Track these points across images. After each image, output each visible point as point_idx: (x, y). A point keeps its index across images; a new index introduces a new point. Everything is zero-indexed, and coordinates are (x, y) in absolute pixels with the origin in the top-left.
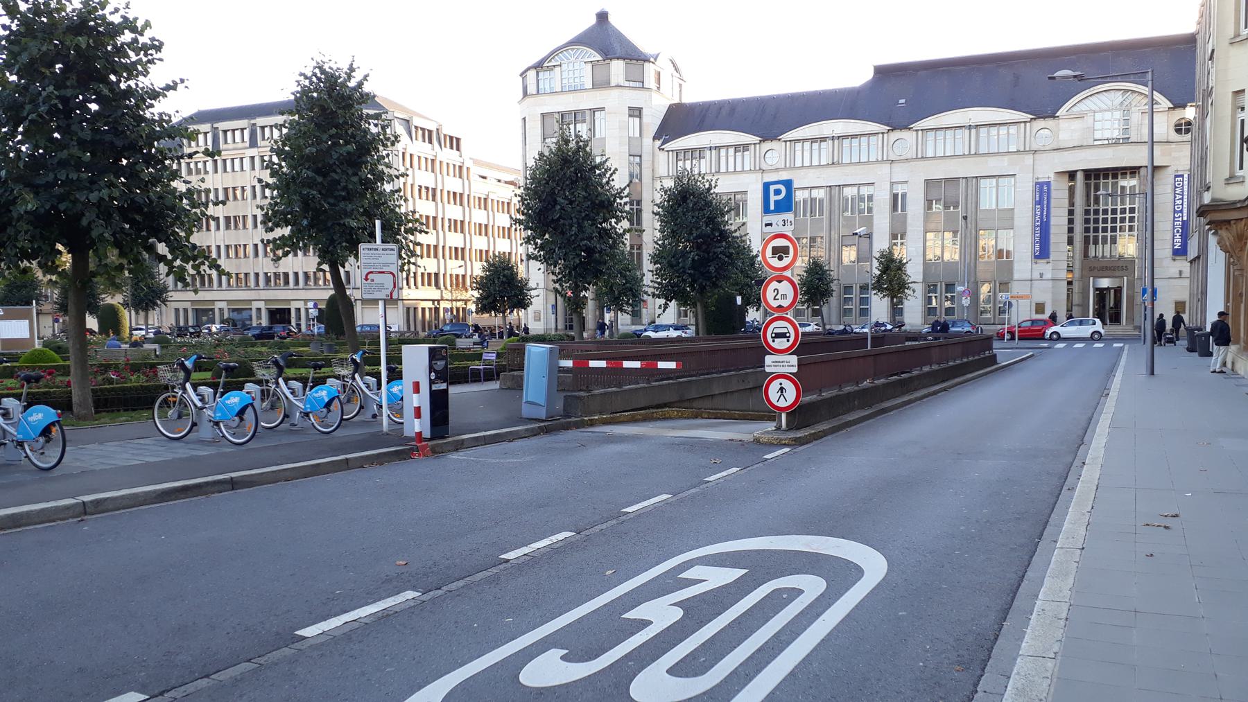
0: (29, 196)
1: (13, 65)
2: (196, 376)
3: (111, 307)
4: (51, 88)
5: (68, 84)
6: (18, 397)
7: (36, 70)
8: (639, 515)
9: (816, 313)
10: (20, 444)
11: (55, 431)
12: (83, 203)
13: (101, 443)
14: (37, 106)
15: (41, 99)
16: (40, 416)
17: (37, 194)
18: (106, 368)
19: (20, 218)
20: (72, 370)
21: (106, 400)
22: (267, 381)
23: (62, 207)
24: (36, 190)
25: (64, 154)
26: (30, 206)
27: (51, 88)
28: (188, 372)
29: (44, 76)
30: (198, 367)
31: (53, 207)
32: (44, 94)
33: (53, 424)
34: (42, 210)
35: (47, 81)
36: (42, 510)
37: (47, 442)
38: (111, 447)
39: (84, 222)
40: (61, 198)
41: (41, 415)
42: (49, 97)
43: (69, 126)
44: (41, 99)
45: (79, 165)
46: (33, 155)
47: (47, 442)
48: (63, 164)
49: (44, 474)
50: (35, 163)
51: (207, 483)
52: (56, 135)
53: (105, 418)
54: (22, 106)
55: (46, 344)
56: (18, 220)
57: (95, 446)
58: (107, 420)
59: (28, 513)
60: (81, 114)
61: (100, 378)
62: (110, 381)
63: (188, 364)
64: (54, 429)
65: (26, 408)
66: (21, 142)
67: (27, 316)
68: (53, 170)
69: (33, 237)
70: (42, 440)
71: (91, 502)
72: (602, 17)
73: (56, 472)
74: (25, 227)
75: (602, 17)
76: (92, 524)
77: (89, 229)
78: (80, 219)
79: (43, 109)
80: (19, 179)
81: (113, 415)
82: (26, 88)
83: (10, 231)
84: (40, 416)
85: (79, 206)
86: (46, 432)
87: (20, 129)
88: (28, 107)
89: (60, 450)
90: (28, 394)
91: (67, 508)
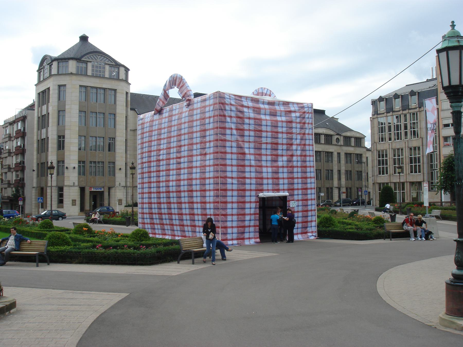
72: (84, 39)
75: (84, 39)
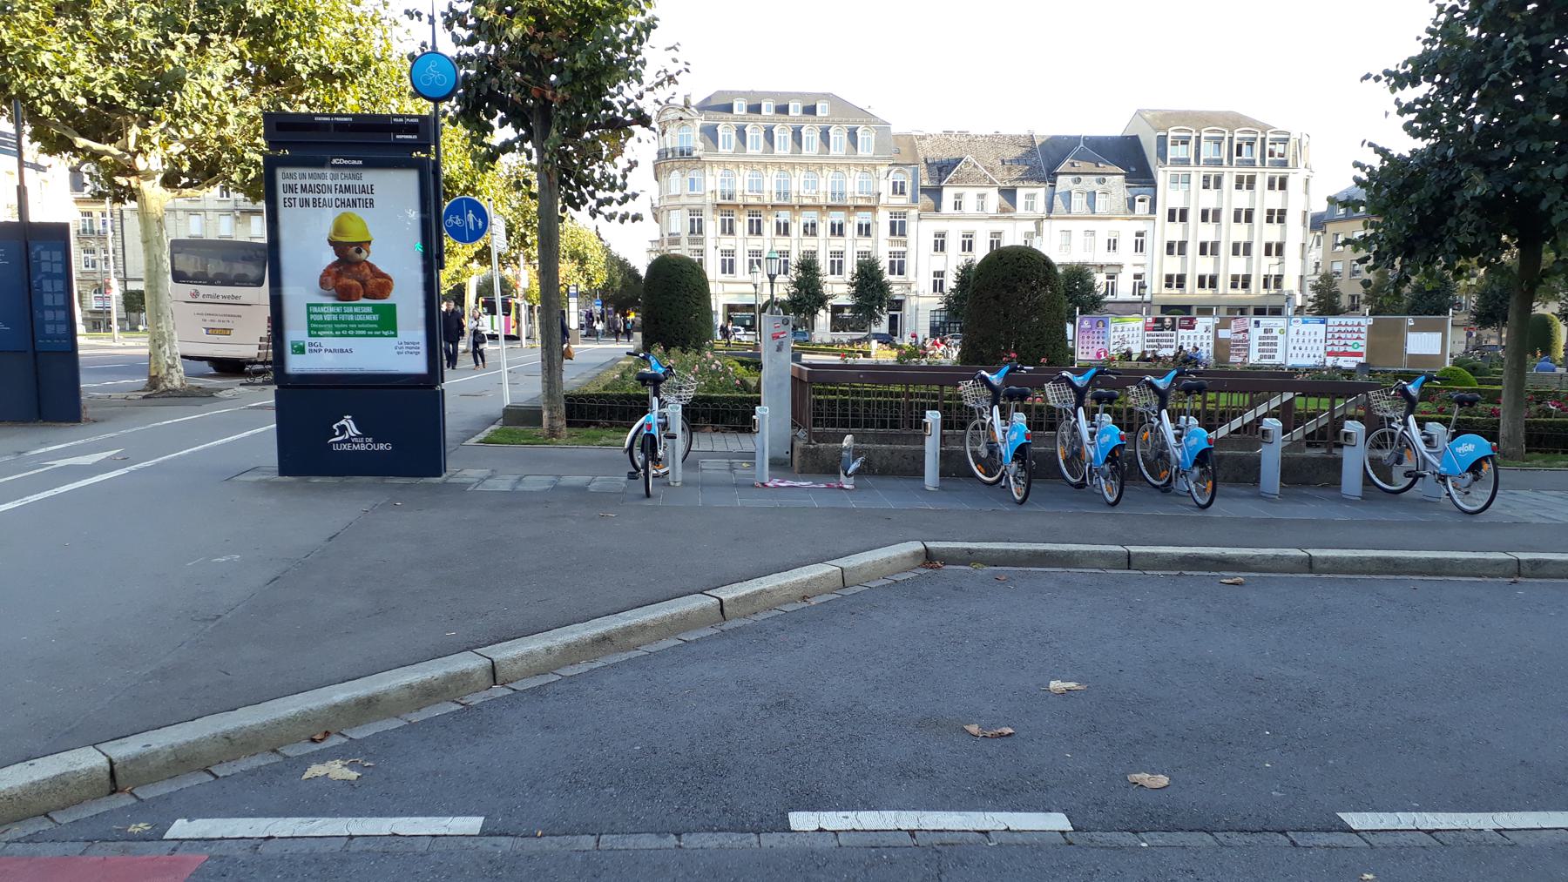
0: (1478, 178)
1: (1476, 16)
2: (1422, 406)
3: (1543, 318)
4: (1520, 37)
5: (1543, 27)
6: (1445, 422)
7: (1505, 17)
8: (1378, 846)
9: (265, 189)
10: (1443, 478)
11: (1487, 467)
12: (1545, 181)
13: (1536, 490)
14: (1501, 62)
15: (1506, 54)
16: (1470, 448)
17: (1487, 174)
18: (1540, 397)
19: (1465, 205)
20: (1504, 395)
21: (1541, 437)
22: (1391, 420)
23: (1519, 186)
24: (1487, 168)
25: (1526, 121)
26: (1479, 190)
27: (1520, 37)
28: (1162, 396)
29: (1512, 22)
30: (1426, 395)
31: (1507, 190)
32: (1511, 46)
33: (1485, 459)
34: (1493, 194)
35: (1516, 29)
36: (1469, 560)
37: (1475, 479)
38: (1549, 497)
39: (1544, 206)
40: (1517, 176)
41: (1472, 446)
42: (1516, 49)
43: (1537, 82)
44: (1506, 54)
45: (1546, 132)
46: (1487, 125)
47: (1475, 479)
48: (1524, 133)
49: (1468, 518)
50: (1487, 133)
51: (1092, 554)
52: (1519, 97)
53: (1539, 459)
54: (1481, 66)
55: (1456, 363)
56: (1461, 209)
57: (1529, 493)
58: (1540, 462)
59: (1452, 561)
60: (1556, 64)
61: (1533, 408)
62: (1548, 413)
63: (1412, 389)
64: (1486, 466)
65: (1454, 436)
66: (1475, 112)
67: (1440, 328)
68: (1510, 142)
69: (1478, 229)
70: (1469, 476)
71: (1528, 561)
73: (1482, 518)
74: (1470, 217)
76: (1527, 589)
77: (1549, 213)
78: (1538, 203)
79: (1507, 65)
80: (1470, 158)
81: (1548, 457)
82: (1488, 42)
83: (1451, 222)
84: (1470, 448)
85: (1540, 185)
86: (1475, 468)
87: (1475, 95)
88: (1489, 66)
89: (1490, 492)
90: (1458, 421)
91: (1498, 563)
